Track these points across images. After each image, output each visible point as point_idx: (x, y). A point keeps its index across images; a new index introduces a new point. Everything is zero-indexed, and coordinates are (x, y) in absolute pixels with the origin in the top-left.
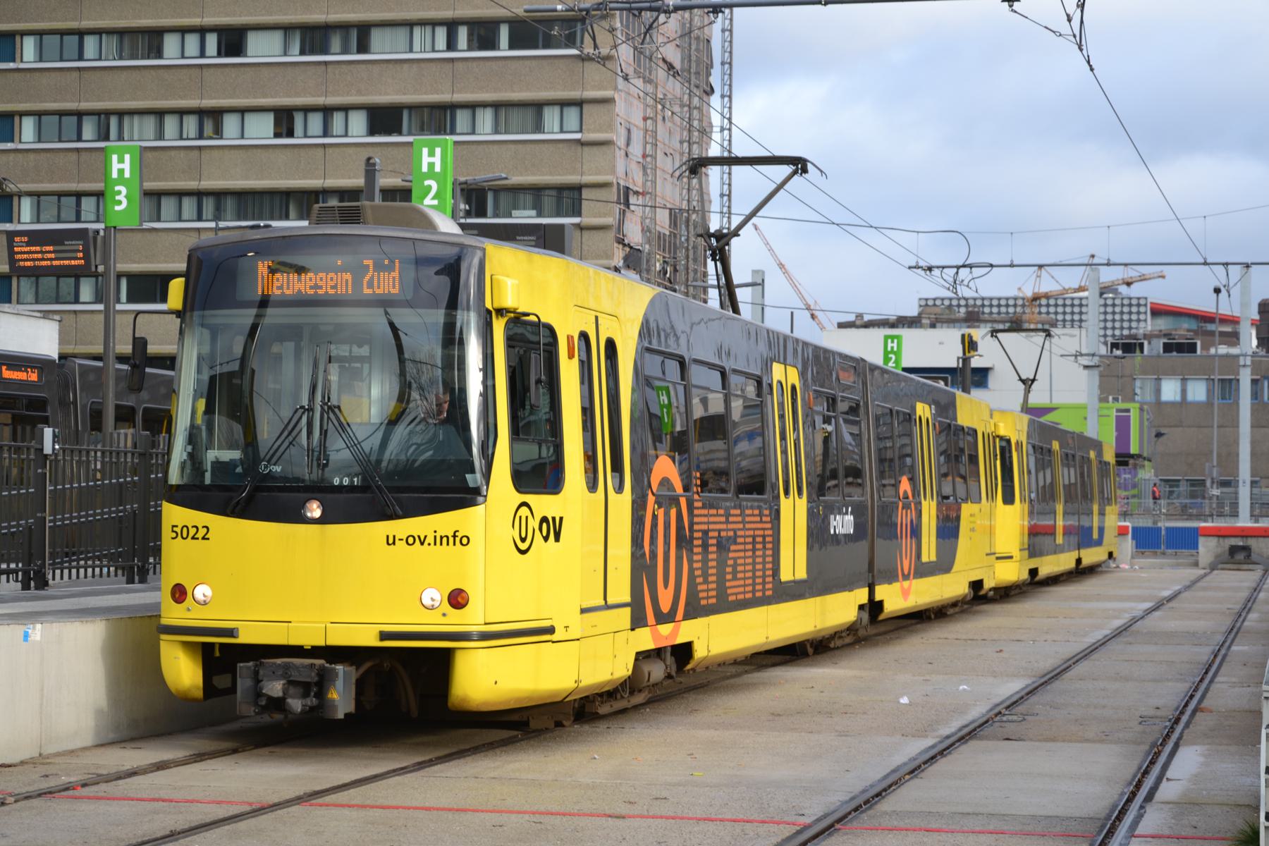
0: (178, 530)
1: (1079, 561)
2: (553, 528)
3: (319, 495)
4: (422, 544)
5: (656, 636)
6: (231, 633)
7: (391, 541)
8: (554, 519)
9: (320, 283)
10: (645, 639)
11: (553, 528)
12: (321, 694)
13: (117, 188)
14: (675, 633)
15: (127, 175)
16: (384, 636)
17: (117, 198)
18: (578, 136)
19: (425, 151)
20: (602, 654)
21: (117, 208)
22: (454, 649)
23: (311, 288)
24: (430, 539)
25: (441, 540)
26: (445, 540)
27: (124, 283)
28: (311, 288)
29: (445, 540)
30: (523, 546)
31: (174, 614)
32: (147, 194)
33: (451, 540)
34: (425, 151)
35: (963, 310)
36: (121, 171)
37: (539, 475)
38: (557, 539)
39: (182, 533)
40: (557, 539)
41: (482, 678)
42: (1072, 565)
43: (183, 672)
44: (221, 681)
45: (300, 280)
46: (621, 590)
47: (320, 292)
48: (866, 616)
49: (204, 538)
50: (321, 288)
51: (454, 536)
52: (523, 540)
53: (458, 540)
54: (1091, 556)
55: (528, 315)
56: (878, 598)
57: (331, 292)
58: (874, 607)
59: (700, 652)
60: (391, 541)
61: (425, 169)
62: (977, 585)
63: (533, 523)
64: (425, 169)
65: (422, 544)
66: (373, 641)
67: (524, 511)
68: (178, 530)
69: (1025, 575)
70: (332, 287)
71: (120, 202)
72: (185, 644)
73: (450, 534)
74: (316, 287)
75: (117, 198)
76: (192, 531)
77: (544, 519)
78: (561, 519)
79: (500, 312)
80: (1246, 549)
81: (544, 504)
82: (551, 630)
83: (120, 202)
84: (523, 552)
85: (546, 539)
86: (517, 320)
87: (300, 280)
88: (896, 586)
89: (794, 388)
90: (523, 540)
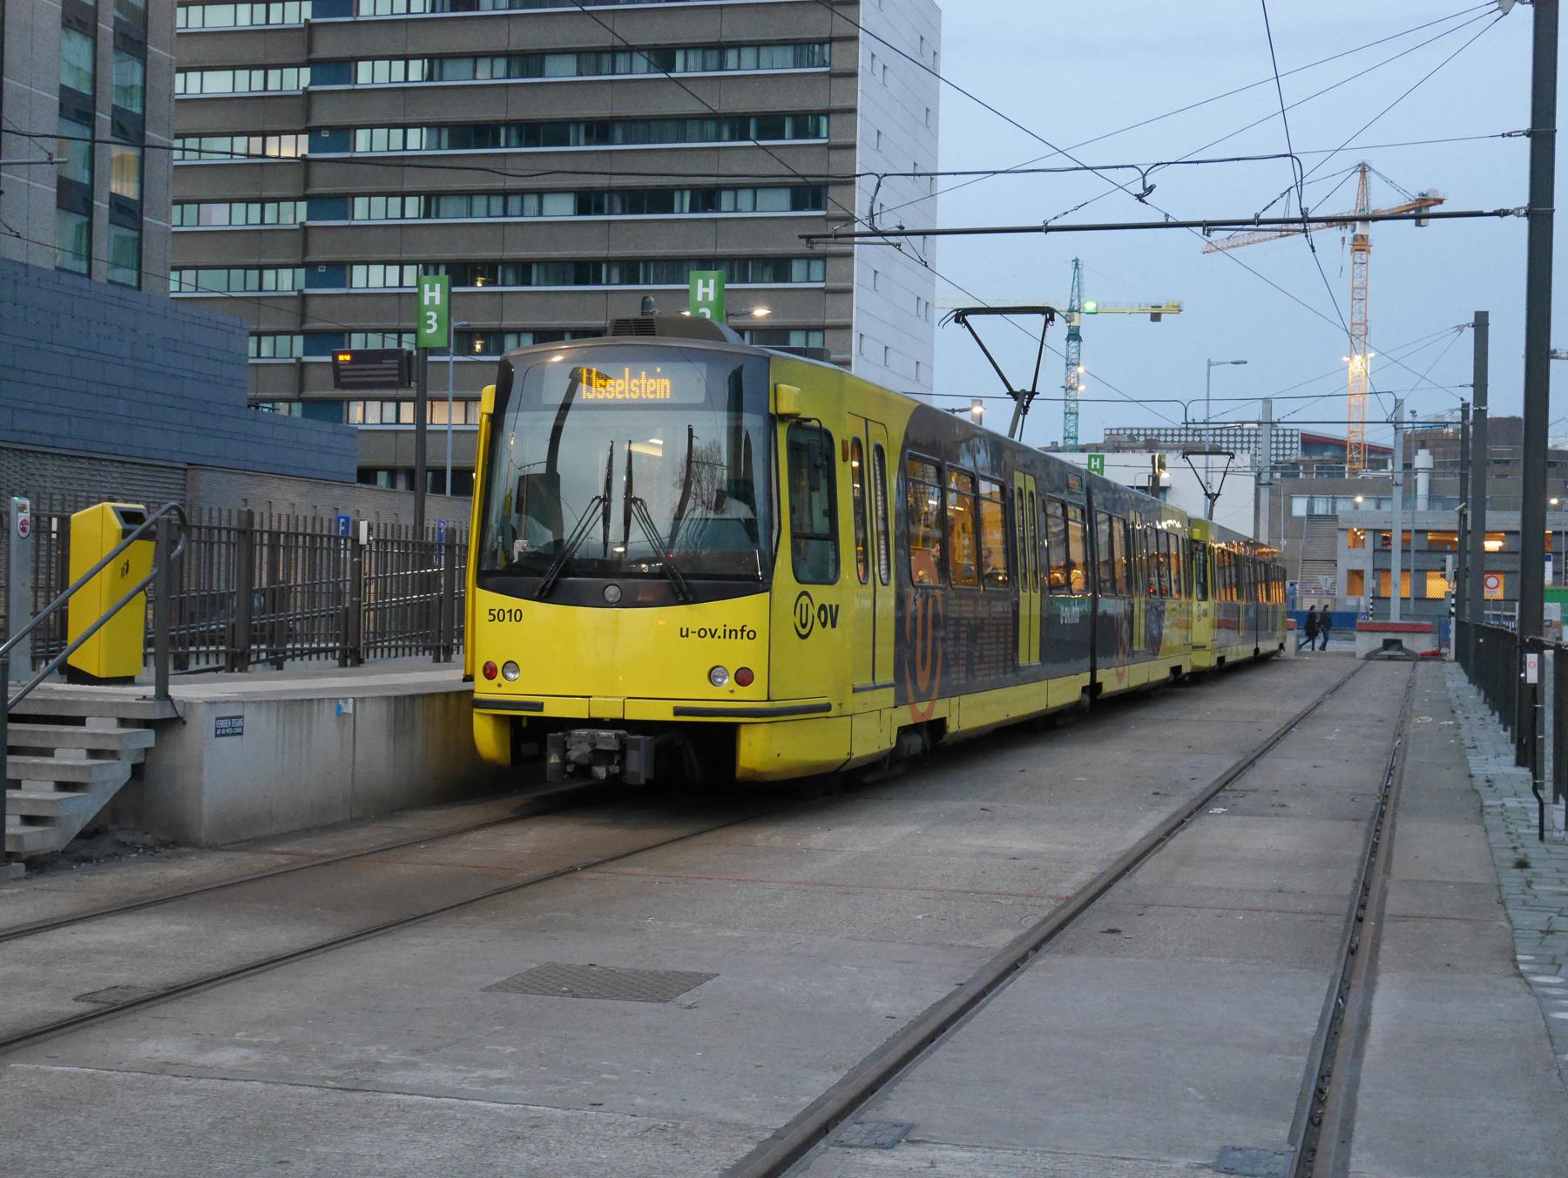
1: (1257, 650)
2: (830, 616)
3: (616, 581)
5: (914, 711)
6: (540, 707)
10: (905, 716)
11: (830, 616)
12: (622, 763)
14: (931, 710)
15: (437, 302)
16: (678, 712)
18: (822, 285)
19: (700, 282)
20: (871, 732)
22: (738, 725)
27: (430, 474)
30: (804, 632)
31: (484, 688)
32: (458, 332)
35: (1142, 439)
37: (817, 565)
38: (834, 625)
39: (496, 616)
40: (834, 625)
41: (758, 750)
42: (1252, 654)
43: (486, 736)
44: (528, 749)
46: (886, 674)
48: (1087, 698)
52: (804, 626)
54: (1267, 646)
55: (809, 420)
56: (1098, 680)
58: (1094, 688)
59: (952, 727)
62: (1176, 670)
63: (813, 611)
64: (700, 298)
66: (669, 716)
67: (805, 600)
69: (1214, 662)
71: (431, 326)
72: (495, 716)
77: (823, 607)
79: (784, 417)
80: (1398, 642)
82: (827, 708)
83: (431, 326)
84: (803, 637)
85: (824, 625)
86: (797, 423)
88: (1113, 670)
89: (48, 752)
90: (804, 626)
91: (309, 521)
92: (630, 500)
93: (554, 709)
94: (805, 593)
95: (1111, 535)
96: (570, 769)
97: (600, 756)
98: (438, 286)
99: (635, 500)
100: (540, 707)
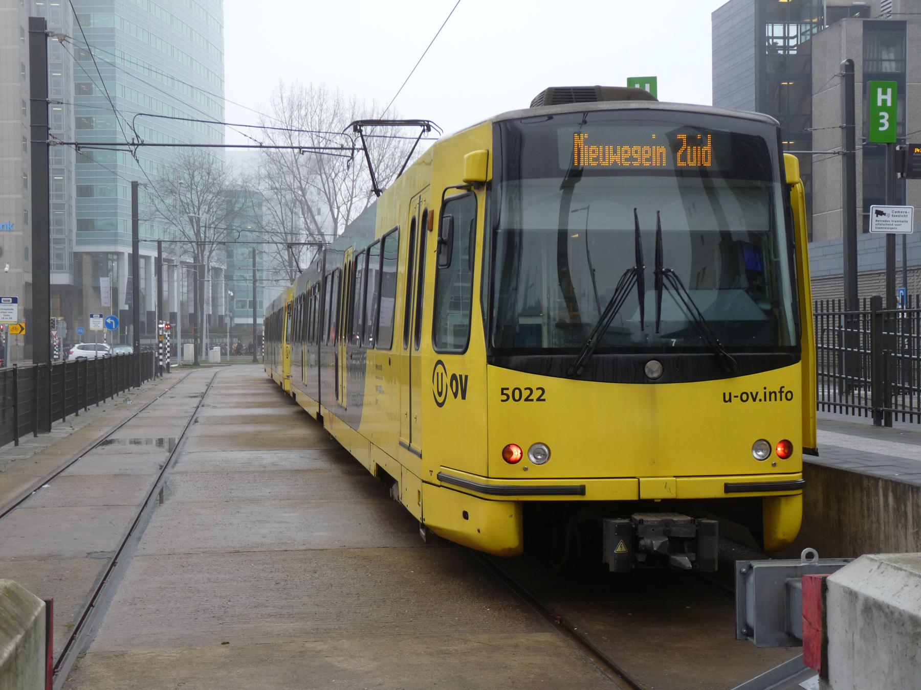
0: (510, 392)
4: (754, 400)
6: (581, 490)
7: (727, 398)
8: (461, 376)
9: (635, 156)
11: (460, 385)
13: (881, 114)
16: (728, 488)
17: (881, 121)
19: (880, 90)
21: (881, 129)
23: (626, 160)
24: (761, 396)
25: (770, 396)
26: (773, 395)
28: (626, 160)
29: (773, 395)
30: (440, 400)
33: (778, 395)
34: (880, 90)
36: (884, 101)
38: (464, 397)
40: (464, 397)
45: (615, 152)
47: (636, 164)
49: (539, 399)
50: (636, 160)
51: (781, 392)
52: (440, 394)
53: (783, 395)
57: (647, 164)
60: (728, 398)
61: (879, 103)
63: (447, 380)
64: (879, 103)
65: (754, 400)
68: (510, 392)
70: (647, 160)
71: (883, 125)
73: (777, 390)
74: (631, 159)
75: (881, 121)
76: (526, 394)
78: (466, 377)
81: (454, 364)
83: (883, 125)
85: (455, 395)
87: (615, 152)
90: (440, 394)
91: (836, 302)
92: (660, 273)
93: (596, 492)
94: (440, 362)
95: (828, 323)
96: (641, 558)
97: (677, 544)
98: (889, 91)
99: (665, 273)
100: (581, 490)
